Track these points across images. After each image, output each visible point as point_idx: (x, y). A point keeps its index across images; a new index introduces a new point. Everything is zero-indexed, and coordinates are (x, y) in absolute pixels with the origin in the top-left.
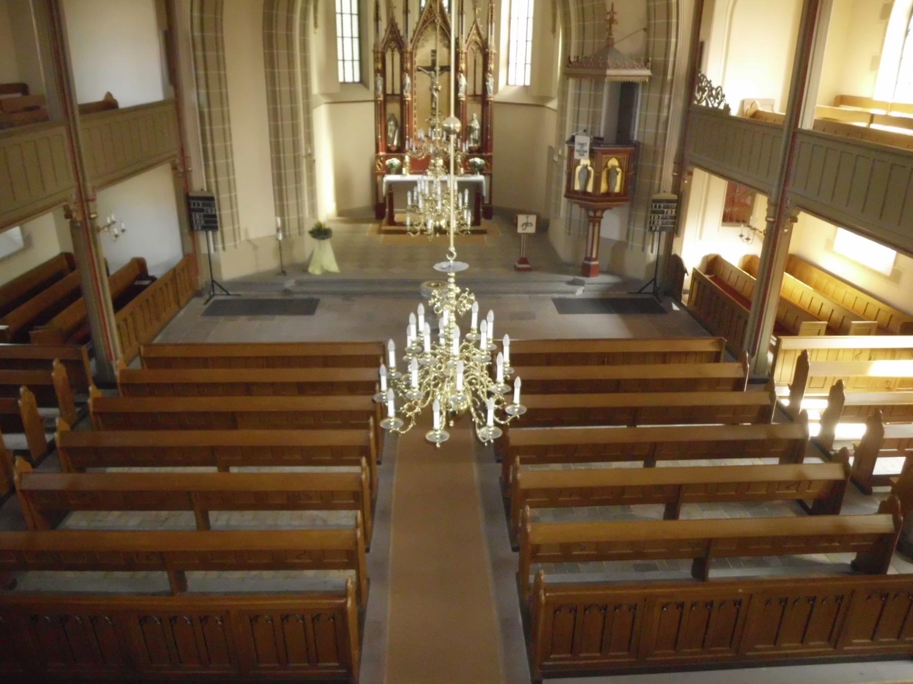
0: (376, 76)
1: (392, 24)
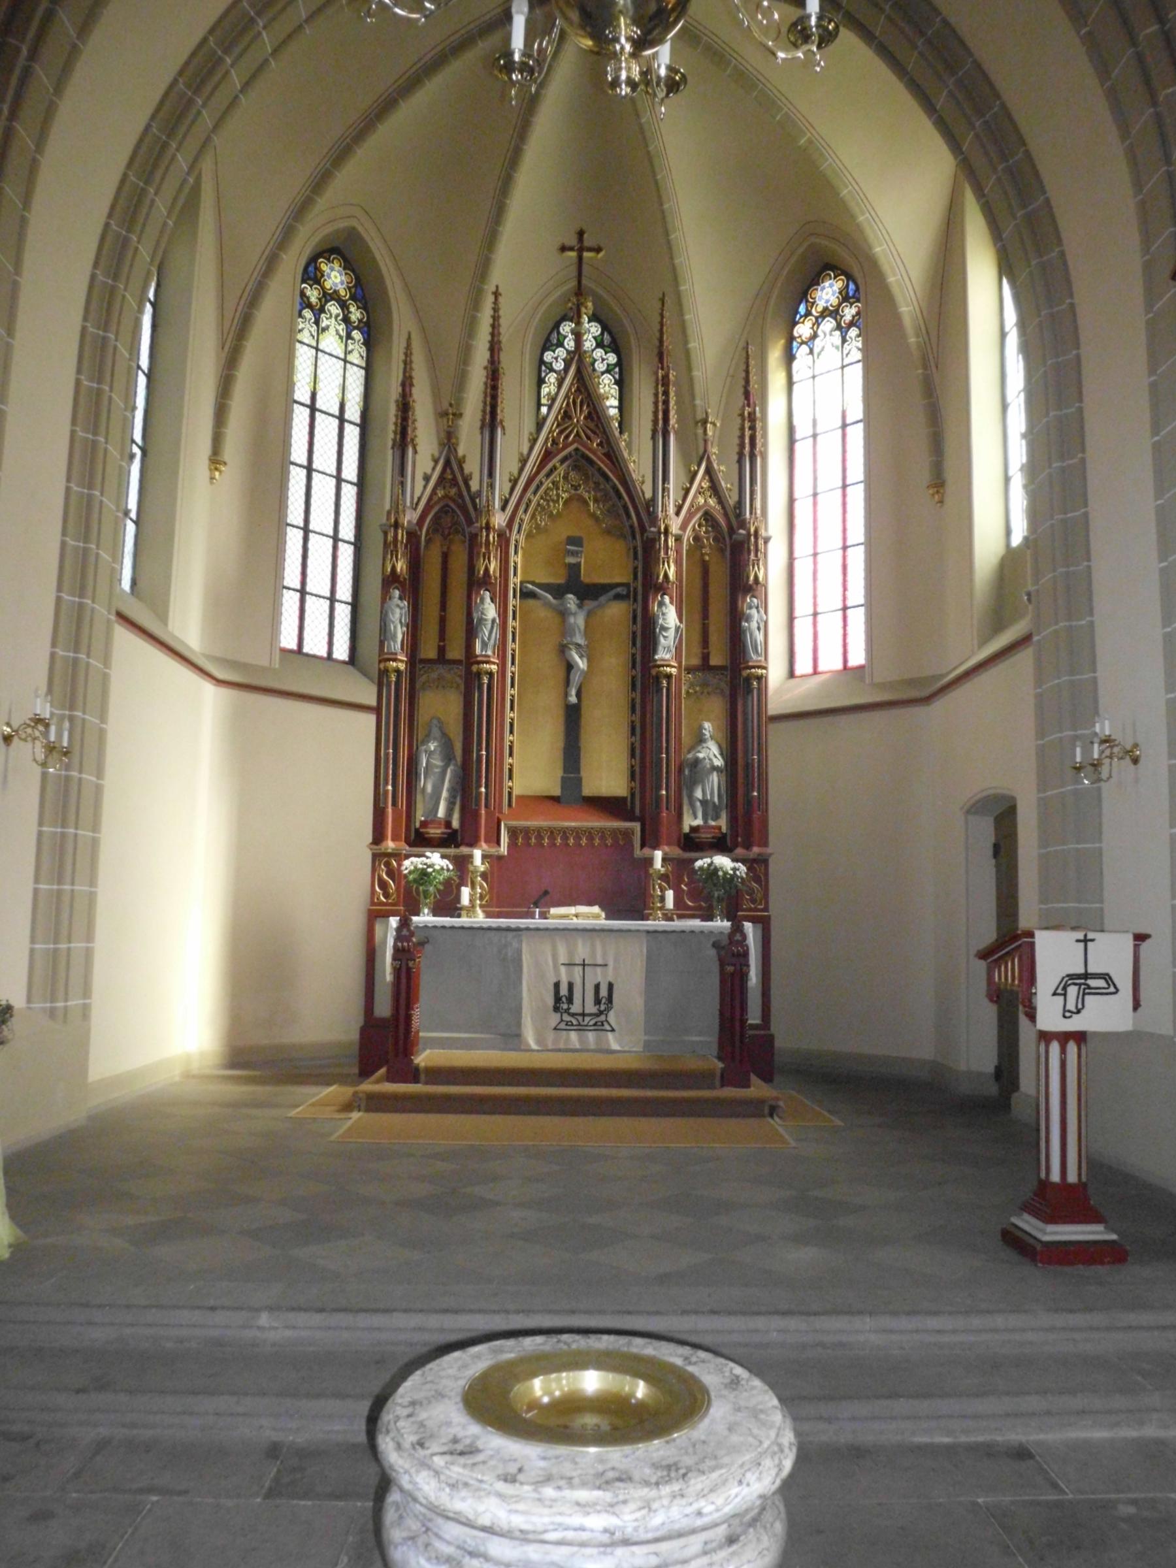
0: (385, 596)
1: (451, 469)
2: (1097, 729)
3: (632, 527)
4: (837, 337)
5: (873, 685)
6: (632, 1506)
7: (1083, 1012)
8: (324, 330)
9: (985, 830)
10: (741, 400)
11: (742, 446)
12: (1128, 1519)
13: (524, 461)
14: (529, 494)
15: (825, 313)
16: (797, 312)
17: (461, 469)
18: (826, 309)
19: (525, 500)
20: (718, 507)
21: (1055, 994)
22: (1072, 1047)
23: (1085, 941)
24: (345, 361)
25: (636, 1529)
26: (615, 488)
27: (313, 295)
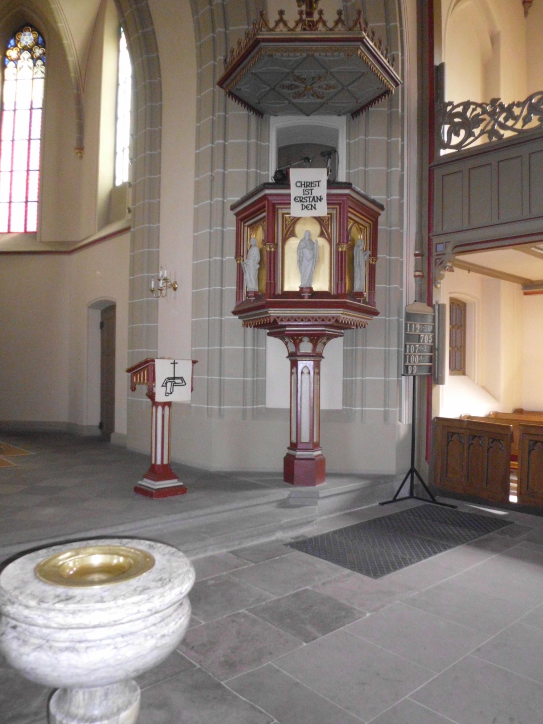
2: (161, 273)
5: (41, 242)
6: (157, 598)
7: (173, 393)
9: (97, 316)
12: (213, 585)
15: (25, 48)
16: (9, 43)
21: (162, 386)
22: (167, 408)
23: (174, 363)
25: (160, 606)
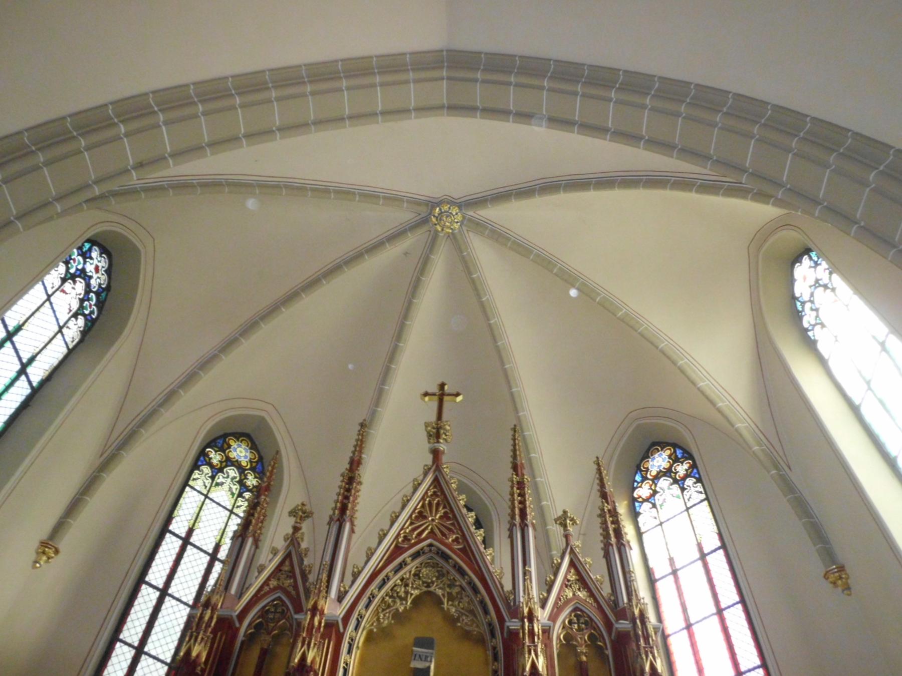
3: (490, 624)
4: (676, 488)
8: (217, 484)
10: (599, 501)
11: (606, 536)
13: (370, 555)
14: (373, 587)
17: (301, 561)
18: (658, 473)
19: (368, 593)
20: (591, 601)
24: (231, 512)
26: (471, 583)
27: (216, 457)
